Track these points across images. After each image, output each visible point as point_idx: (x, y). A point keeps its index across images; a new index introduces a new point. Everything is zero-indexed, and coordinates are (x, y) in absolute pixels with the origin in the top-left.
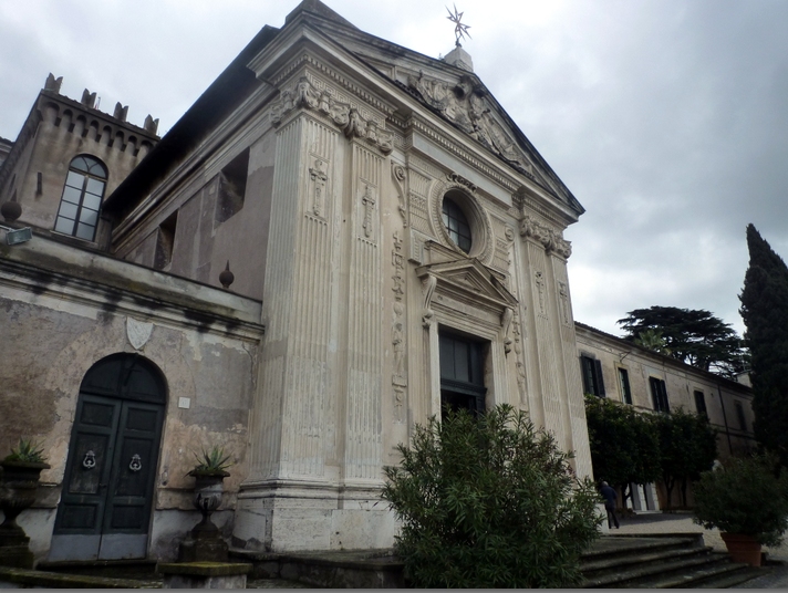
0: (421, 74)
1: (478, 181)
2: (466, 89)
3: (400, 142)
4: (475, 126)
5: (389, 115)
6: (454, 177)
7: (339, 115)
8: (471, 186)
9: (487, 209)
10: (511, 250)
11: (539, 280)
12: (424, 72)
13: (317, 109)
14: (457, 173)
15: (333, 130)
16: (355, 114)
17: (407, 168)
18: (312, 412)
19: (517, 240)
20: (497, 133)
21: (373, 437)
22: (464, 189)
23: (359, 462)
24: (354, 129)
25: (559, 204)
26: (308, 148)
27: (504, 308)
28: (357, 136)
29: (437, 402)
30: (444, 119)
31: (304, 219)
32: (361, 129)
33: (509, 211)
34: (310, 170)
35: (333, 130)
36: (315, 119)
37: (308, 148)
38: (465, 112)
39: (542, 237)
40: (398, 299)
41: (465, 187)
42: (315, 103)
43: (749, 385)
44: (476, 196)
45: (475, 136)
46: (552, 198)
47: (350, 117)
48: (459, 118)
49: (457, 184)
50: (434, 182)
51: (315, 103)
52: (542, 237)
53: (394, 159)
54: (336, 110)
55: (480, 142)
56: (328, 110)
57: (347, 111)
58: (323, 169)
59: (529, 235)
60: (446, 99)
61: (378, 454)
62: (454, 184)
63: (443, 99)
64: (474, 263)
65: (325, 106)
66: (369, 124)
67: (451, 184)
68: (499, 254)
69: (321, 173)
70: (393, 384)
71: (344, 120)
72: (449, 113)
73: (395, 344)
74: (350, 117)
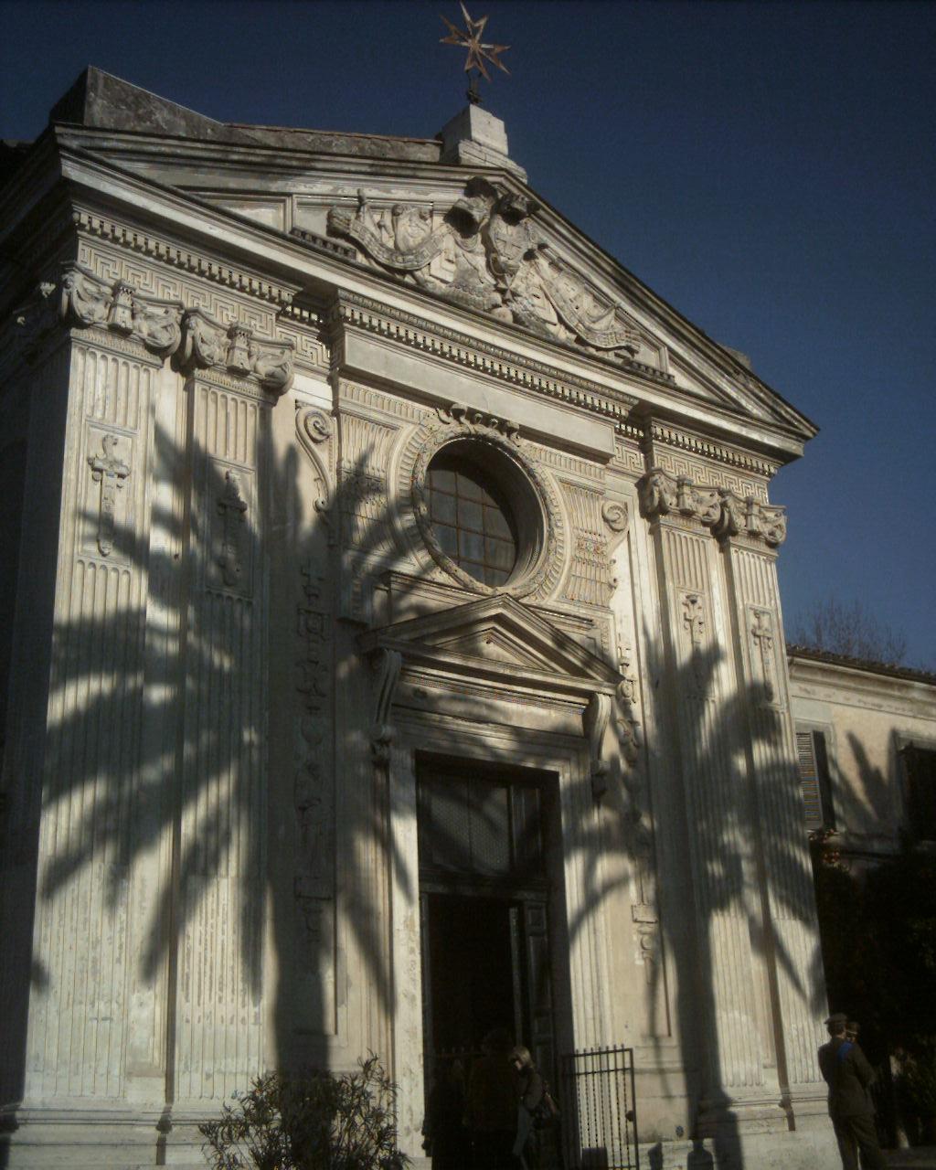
0: (360, 199)
1: (519, 409)
2: (480, 209)
3: (321, 354)
4: (503, 292)
5: (282, 303)
6: (458, 414)
7: (156, 327)
8: (503, 426)
9: (549, 469)
10: (620, 553)
11: (694, 613)
12: (370, 192)
13: (224, 366)
14: (463, 404)
15: (143, 362)
16: (193, 321)
17: (336, 413)
18: (95, 972)
19: (639, 526)
20: (568, 288)
21: (242, 1013)
22: (485, 438)
23: (208, 1066)
24: (195, 350)
25: (745, 424)
26: (88, 411)
27: (591, 696)
28: (203, 366)
29: (412, 1034)
30: (421, 291)
31: (78, 568)
32: (213, 348)
33: (613, 463)
34: (91, 462)
35: (143, 362)
36: (100, 347)
37: (88, 411)
38: (481, 261)
39: (702, 510)
40: (312, 709)
41: (490, 432)
42: (100, 311)
43: (53, 287)
44: (524, 447)
45: (505, 313)
46: (735, 420)
47: (184, 327)
48: (463, 280)
49: (469, 427)
50: (407, 432)
51: (100, 311)
52: (702, 510)
53: (301, 397)
54: (149, 317)
55: (520, 327)
56: (129, 324)
57: (175, 315)
58: (118, 453)
59: (665, 511)
60: (429, 240)
61: (254, 1049)
62: (459, 430)
63: (424, 242)
64: (505, 605)
65: (122, 317)
66: (232, 333)
67: (453, 429)
68: (580, 569)
69: (116, 462)
70: (298, 896)
71: (169, 338)
72: (440, 271)
73: (303, 809)
74: (184, 327)
